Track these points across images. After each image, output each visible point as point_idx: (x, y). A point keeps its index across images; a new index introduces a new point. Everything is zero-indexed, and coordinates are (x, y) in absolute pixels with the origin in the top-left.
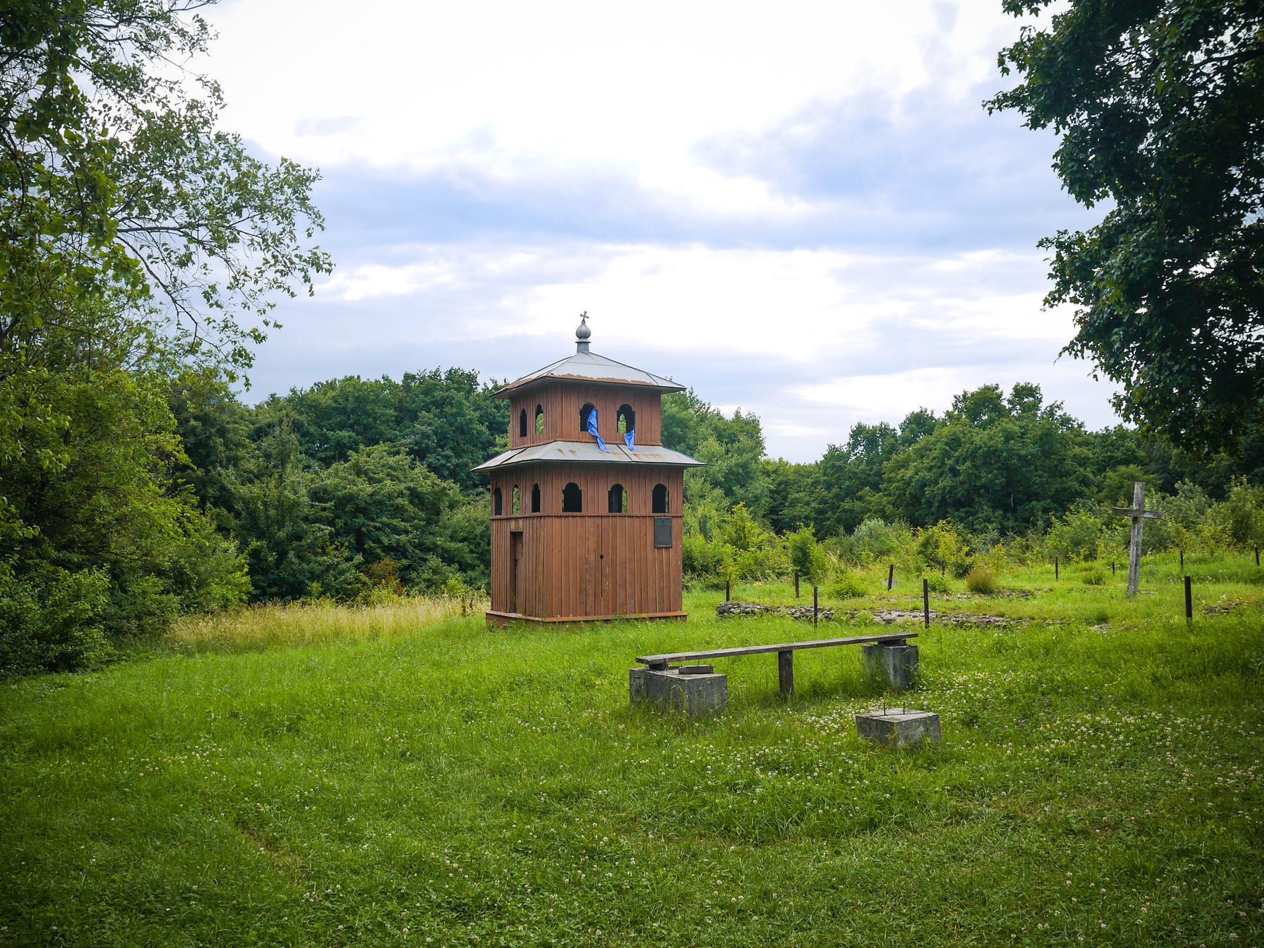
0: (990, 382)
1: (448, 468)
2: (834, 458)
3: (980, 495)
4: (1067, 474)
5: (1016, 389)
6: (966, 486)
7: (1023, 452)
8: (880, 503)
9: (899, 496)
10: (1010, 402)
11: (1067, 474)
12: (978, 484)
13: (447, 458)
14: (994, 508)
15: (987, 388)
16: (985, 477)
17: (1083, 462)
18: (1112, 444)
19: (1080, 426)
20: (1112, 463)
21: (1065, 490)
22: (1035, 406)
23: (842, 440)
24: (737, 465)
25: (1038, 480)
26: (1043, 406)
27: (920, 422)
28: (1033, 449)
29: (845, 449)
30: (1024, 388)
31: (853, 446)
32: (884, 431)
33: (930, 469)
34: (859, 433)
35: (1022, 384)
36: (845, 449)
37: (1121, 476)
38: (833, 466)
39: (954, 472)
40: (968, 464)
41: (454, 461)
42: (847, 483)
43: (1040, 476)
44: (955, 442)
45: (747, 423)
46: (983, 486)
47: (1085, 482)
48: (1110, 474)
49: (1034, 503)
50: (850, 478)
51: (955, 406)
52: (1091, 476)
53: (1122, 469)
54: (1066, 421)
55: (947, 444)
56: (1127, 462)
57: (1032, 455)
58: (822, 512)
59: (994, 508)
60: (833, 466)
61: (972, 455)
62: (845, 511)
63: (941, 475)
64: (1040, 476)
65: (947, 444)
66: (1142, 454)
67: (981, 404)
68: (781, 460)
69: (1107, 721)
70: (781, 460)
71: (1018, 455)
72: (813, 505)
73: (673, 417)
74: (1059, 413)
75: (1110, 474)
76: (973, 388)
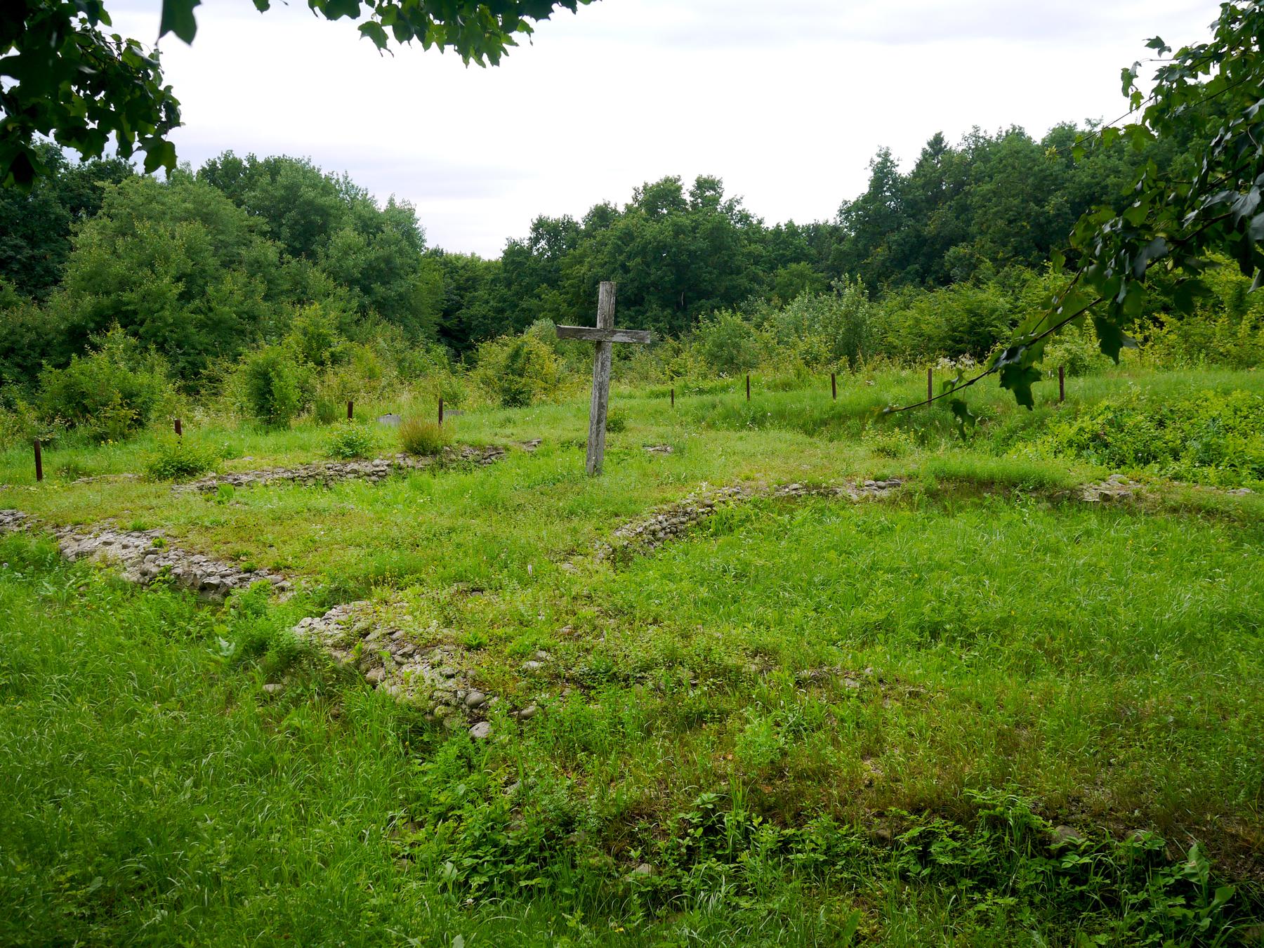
0: (672, 174)
1: (19, 261)
2: (515, 254)
3: (648, 293)
4: (738, 271)
5: (698, 181)
6: (636, 284)
7: (692, 248)
8: (554, 302)
9: (574, 294)
10: (692, 194)
11: (738, 271)
12: (648, 281)
13: (17, 248)
14: (663, 307)
15: (667, 180)
16: (655, 273)
17: (757, 260)
18: (784, 242)
19: (760, 222)
20: (785, 261)
21: (734, 287)
22: (715, 201)
23: (523, 234)
24: (377, 259)
25: (707, 277)
26: (724, 200)
27: (602, 215)
28: (703, 244)
29: (526, 243)
30: (706, 181)
31: (535, 241)
32: (569, 225)
33: (602, 266)
34: (543, 228)
35: (705, 176)
36: (526, 243)
37: (791, 274)
38: (513, 262)
39: (626, 270)
40: (638, 260)
41: (28, 252)
42: (527, 280)
43: (710, 273)
44: (628, 236)
45: (401, 212)
46: (654, 284)
47: (754, 279)
48: (781, 271)
49: (703, 301)
50: (531, 275)
51: (635, 199)
52: (761, 273)
53: (793, 266)
54: (745, 218)
55: (619, 238)
56: (797, 260)
57: (702, 250)
58: (502, 311)
59: (663, 307)
60: (513, 262)
61: (643, 251)
62: (523, 310)
63: (613, 272)
64: (710, 273)
65: (619, 238)
66: (813, 251)
67: (661, 196)
68: (473, 254)
69: (1003, 303)
70: (473, 254)
71: (687, 250)
72: (492, 303)
73: (310, 203)
74: (738, 208)
75: (781, 271)
76: (654, 179)
